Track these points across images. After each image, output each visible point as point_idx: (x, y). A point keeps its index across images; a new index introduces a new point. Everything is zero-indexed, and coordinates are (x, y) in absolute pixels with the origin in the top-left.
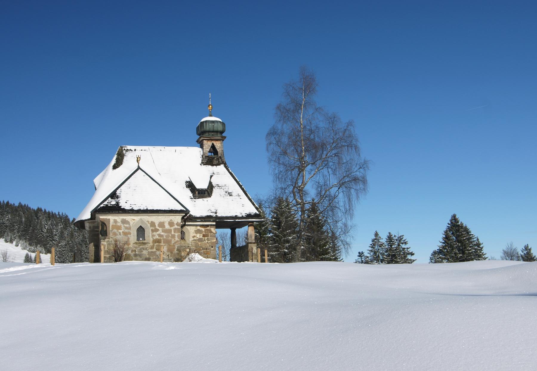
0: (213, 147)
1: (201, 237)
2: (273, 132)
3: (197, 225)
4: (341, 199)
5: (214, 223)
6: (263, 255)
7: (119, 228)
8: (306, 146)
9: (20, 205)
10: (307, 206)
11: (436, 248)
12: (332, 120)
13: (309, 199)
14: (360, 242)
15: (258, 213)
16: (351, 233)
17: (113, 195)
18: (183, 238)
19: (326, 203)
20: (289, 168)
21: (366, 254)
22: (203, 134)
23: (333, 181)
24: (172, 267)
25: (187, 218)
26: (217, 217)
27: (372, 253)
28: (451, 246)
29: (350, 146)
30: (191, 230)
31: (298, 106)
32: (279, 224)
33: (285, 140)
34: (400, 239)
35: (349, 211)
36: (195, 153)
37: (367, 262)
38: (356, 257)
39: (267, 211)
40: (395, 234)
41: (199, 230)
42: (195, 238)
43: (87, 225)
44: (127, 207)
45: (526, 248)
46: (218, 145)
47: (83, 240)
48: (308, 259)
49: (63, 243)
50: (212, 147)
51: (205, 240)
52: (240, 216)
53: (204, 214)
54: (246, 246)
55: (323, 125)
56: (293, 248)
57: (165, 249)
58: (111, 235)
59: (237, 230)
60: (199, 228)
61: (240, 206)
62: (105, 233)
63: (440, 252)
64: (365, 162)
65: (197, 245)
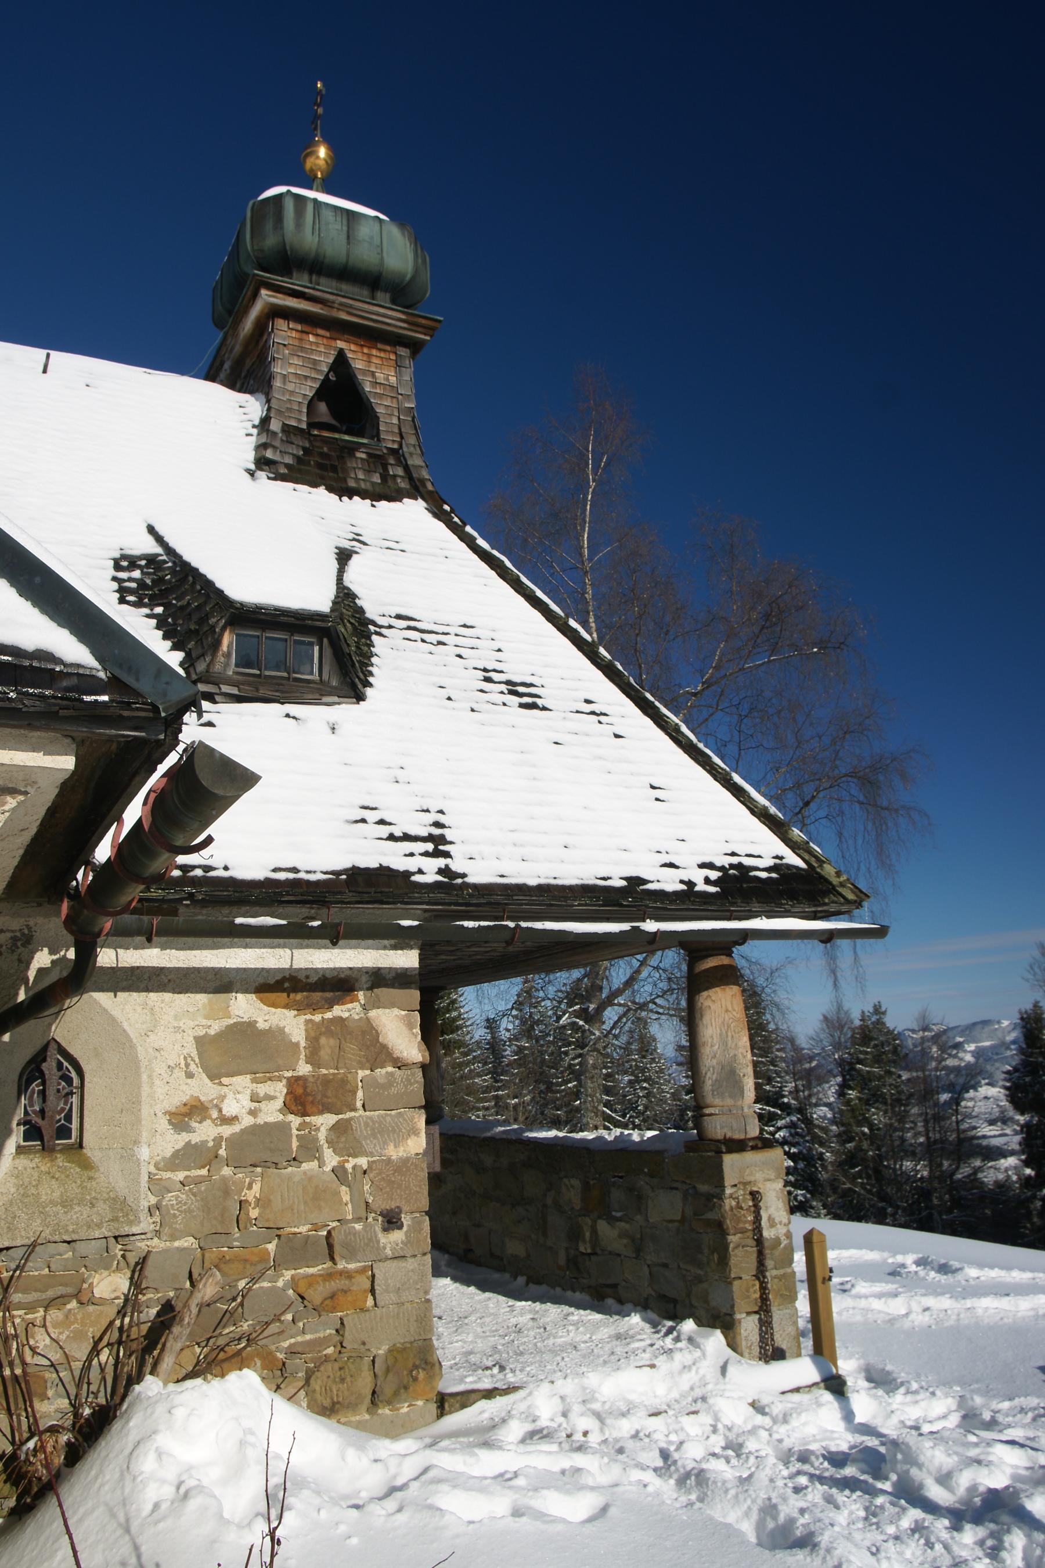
1: (272, 1113)
3: (221, 983)
5: (408, 959)
15: (793, 860)
26: (454, 894)
27: (517, 1022)
41: (245, 1030)
42: (205, 1132)
50: (333, 368)
51: (310, 1149)
52: (670, 882)
60: (244, 1006)
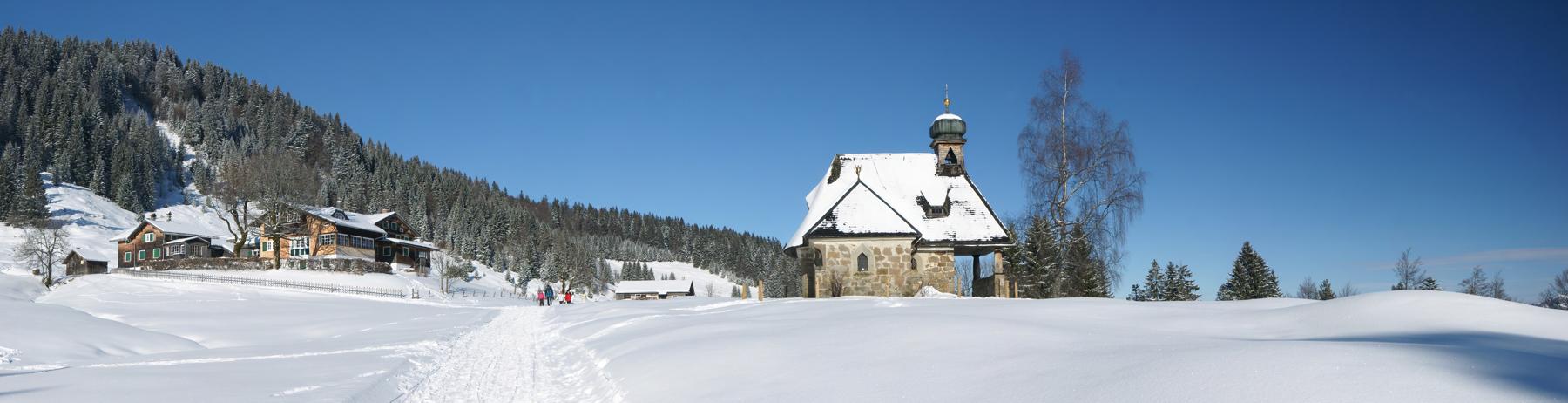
0: (951, 152)
2: (1027, 134)
4: (1111, 220)
6: (1012, 289)
7: (836, 256)
8: (1063, 153)
9: (725, 230)
10: (1069, 228)
11: (1225, 282)
12: (1102, 119)
13: (1071, 219)
14: (1132, 270)
16: (1123, 261)
17: (829, 216)
18: (914, 267)
19: (1092, 225)
20: (1047, 179)
21: (1142, 288)
22: (938, 136)
23: (1102, 197)
24: (898, 303)
25: (919, 242)
28: (1242, 280)
29: (1123, 152)
30: (923, 258)
31: (1058, 100)
32: (1033, 248)
33: (1042, 143)
34: (1183, 270)
35: (1120, 235)
36: (929, 161)
37: (1142, 299)
38: (1130, 292)
39: (1020, 233)
40: (1177, 263)
43: (799, 252)
44: (846, 231)
45: (1326, 284)
46: (957, 150)
47: (794, 270)
48: (1071, 294)
49: (775, 274)
53: (941, 238)
54: (992, 278)
55: (1088, 123)
56: (1051, 279)
57: (892, 281)
58: (827, 264)
59: (981, 258)
61: (984, 228)
62: (820, 263)
63: (1229, 286)
64: (1142, 174)
65: (931, 277)
